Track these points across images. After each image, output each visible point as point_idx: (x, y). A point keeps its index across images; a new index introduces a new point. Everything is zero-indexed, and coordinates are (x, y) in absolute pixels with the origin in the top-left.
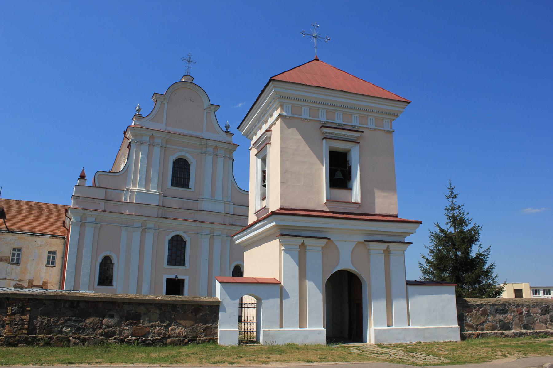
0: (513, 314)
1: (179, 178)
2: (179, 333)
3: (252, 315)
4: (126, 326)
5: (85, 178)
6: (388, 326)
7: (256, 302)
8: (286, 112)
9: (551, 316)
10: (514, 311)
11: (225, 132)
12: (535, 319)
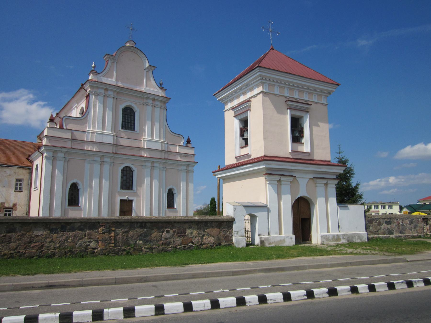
0: (394, 224)
1: (126, 123)
2: (210, 241)
3: (248, 227)
4: (177, 238)
5: (191, 143)
6: (328, 232)
7: (250, 218)
8: (265, 90)
9: (414, 225)
10: (395, 223)
11: (160, 87)
12: (406, 227)
